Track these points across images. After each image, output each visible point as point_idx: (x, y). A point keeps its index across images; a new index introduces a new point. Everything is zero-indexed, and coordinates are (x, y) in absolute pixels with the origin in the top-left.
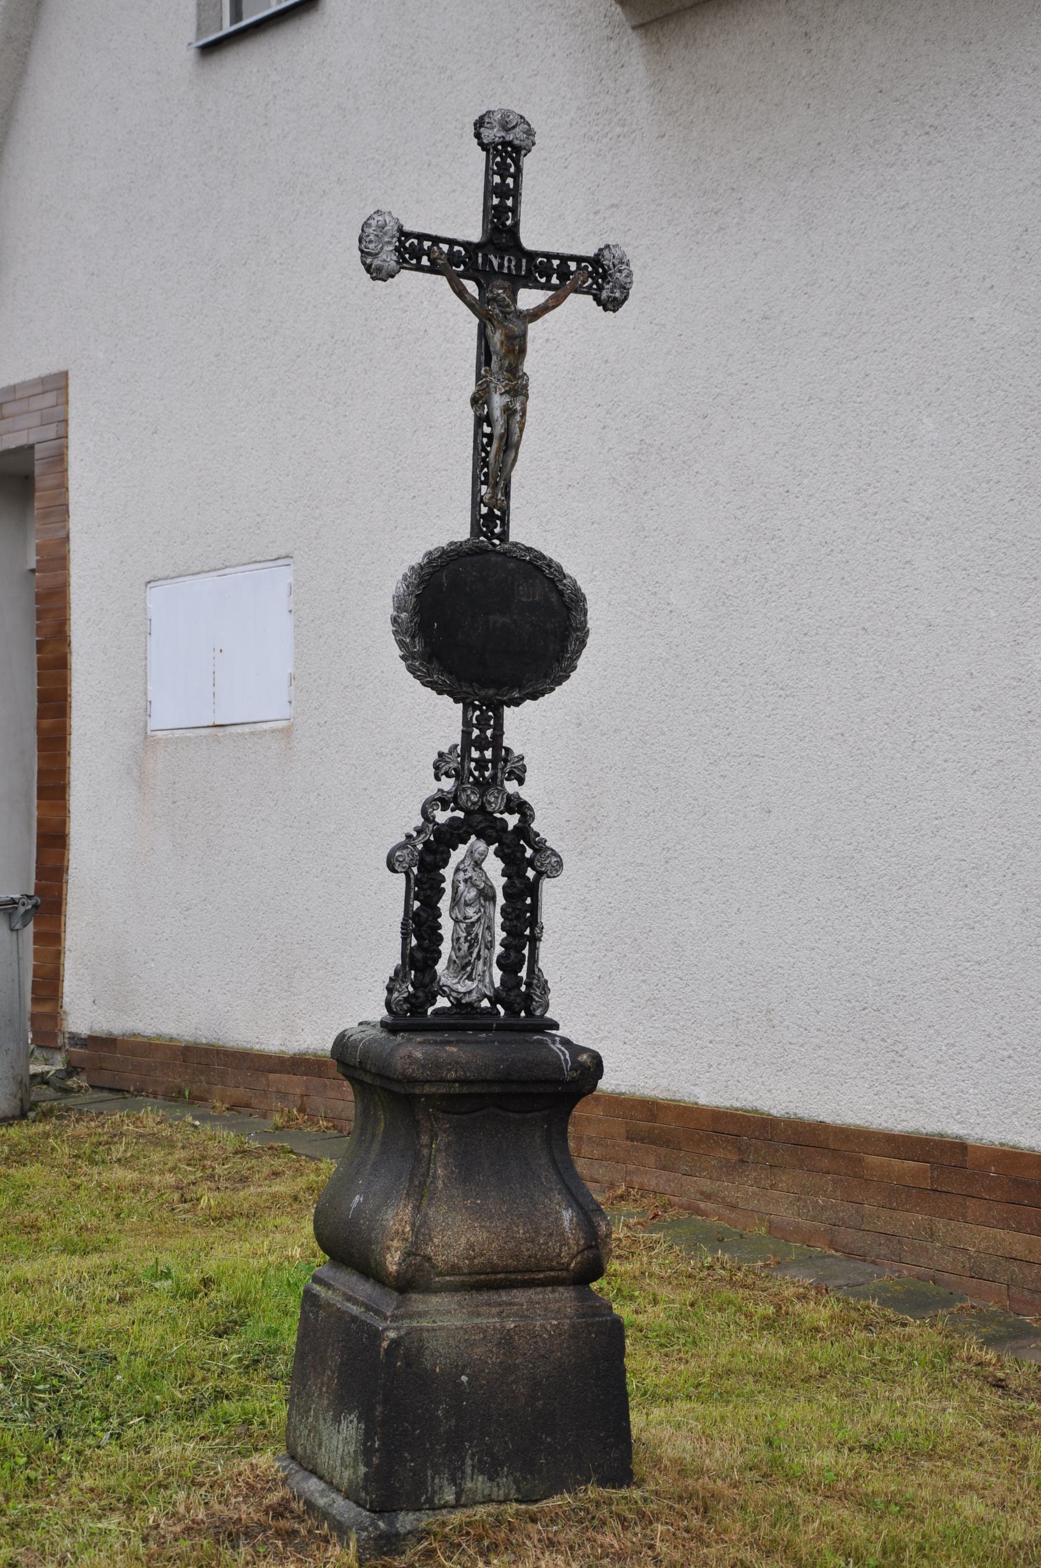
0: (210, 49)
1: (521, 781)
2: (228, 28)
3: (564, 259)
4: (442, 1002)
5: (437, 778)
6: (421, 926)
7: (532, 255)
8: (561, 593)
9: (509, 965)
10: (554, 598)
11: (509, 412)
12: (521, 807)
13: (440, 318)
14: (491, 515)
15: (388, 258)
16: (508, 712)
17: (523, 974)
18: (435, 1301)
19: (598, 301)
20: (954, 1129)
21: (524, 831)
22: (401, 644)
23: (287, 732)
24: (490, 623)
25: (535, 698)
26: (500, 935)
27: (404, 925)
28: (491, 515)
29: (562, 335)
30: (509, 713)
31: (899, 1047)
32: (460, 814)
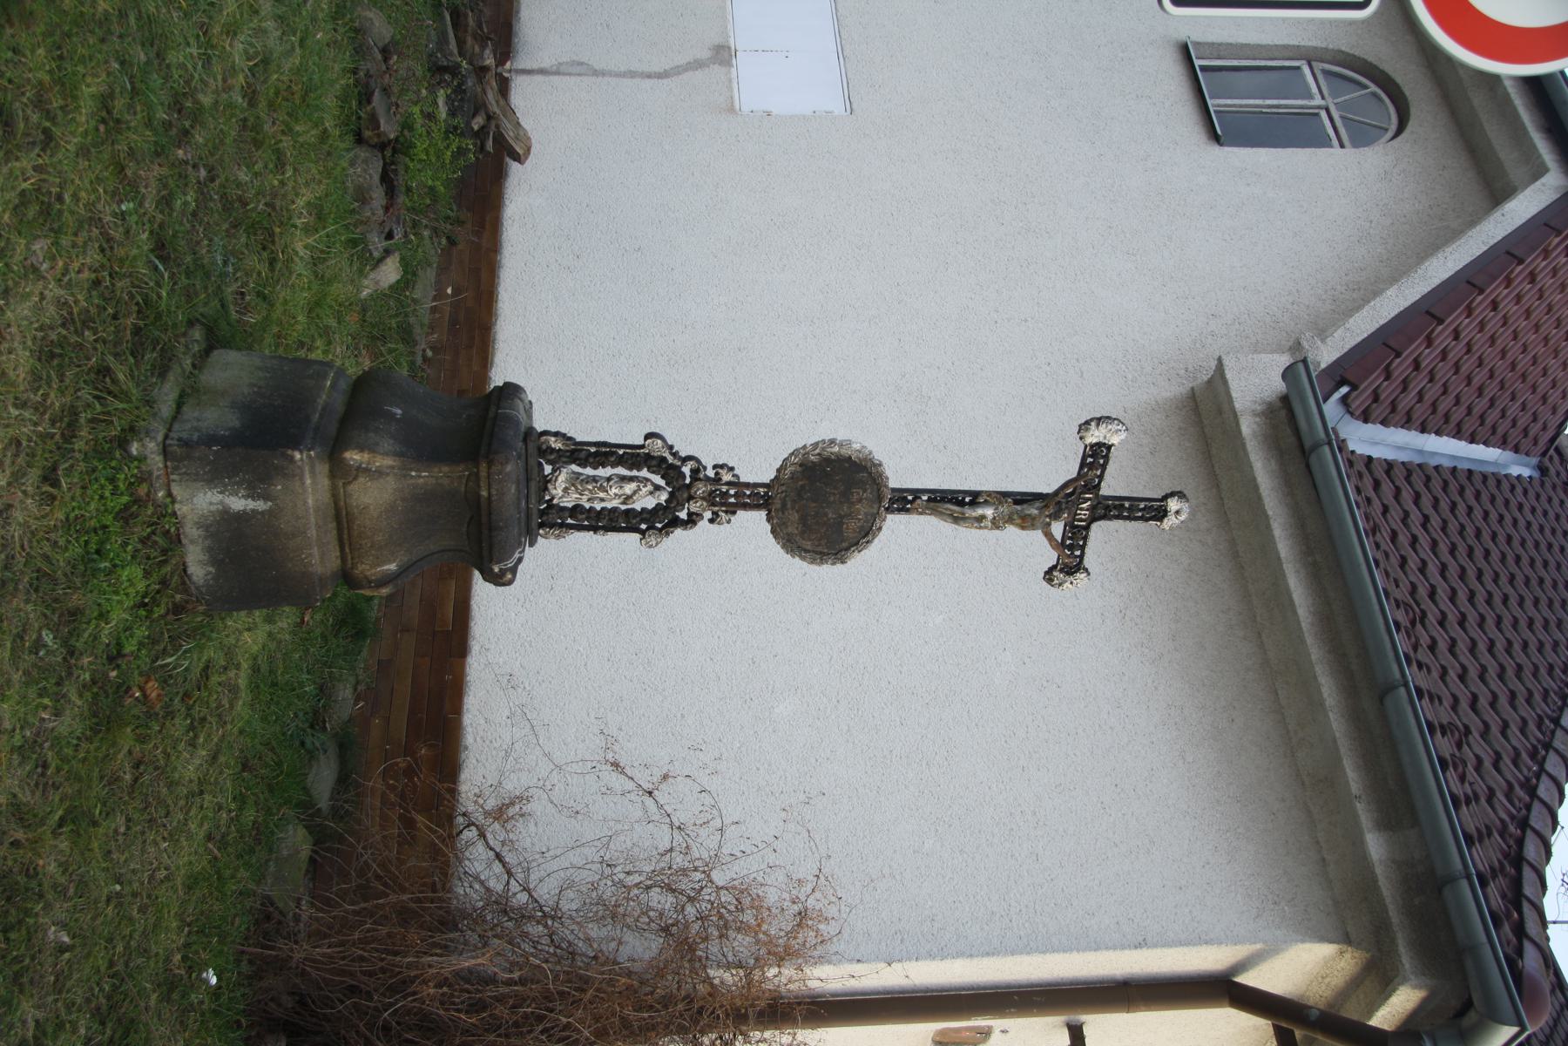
0: (1185, 51)
1: (711, 521)
2: (1197, 63)
3: (1083, 548)
4: (548, 469)
5: (715, 467)
6: (603, 454)
7: (1087, 528)
8: (847, 549)
9: (576, 510)
10: (845, 545)
11: (982, 518)
12: (692, 520)
13: (1049, 471)
14: (904, 501)
15: (1095, 435)
16: (763, 514)
17: (569, 521)
18: (325, 482)
19: (1053, 568)
20: (475, 647)
21: (675, 523)
22: (816, 445)
23: (731, 110)
24: (827, 503)
25: (773, 531)
26: (598, 506)
27: (605, 444)
28: (904, 501)
29: (1034, 548)
30: (761, 515)
31: (527, 605)
32: (688, 481)
